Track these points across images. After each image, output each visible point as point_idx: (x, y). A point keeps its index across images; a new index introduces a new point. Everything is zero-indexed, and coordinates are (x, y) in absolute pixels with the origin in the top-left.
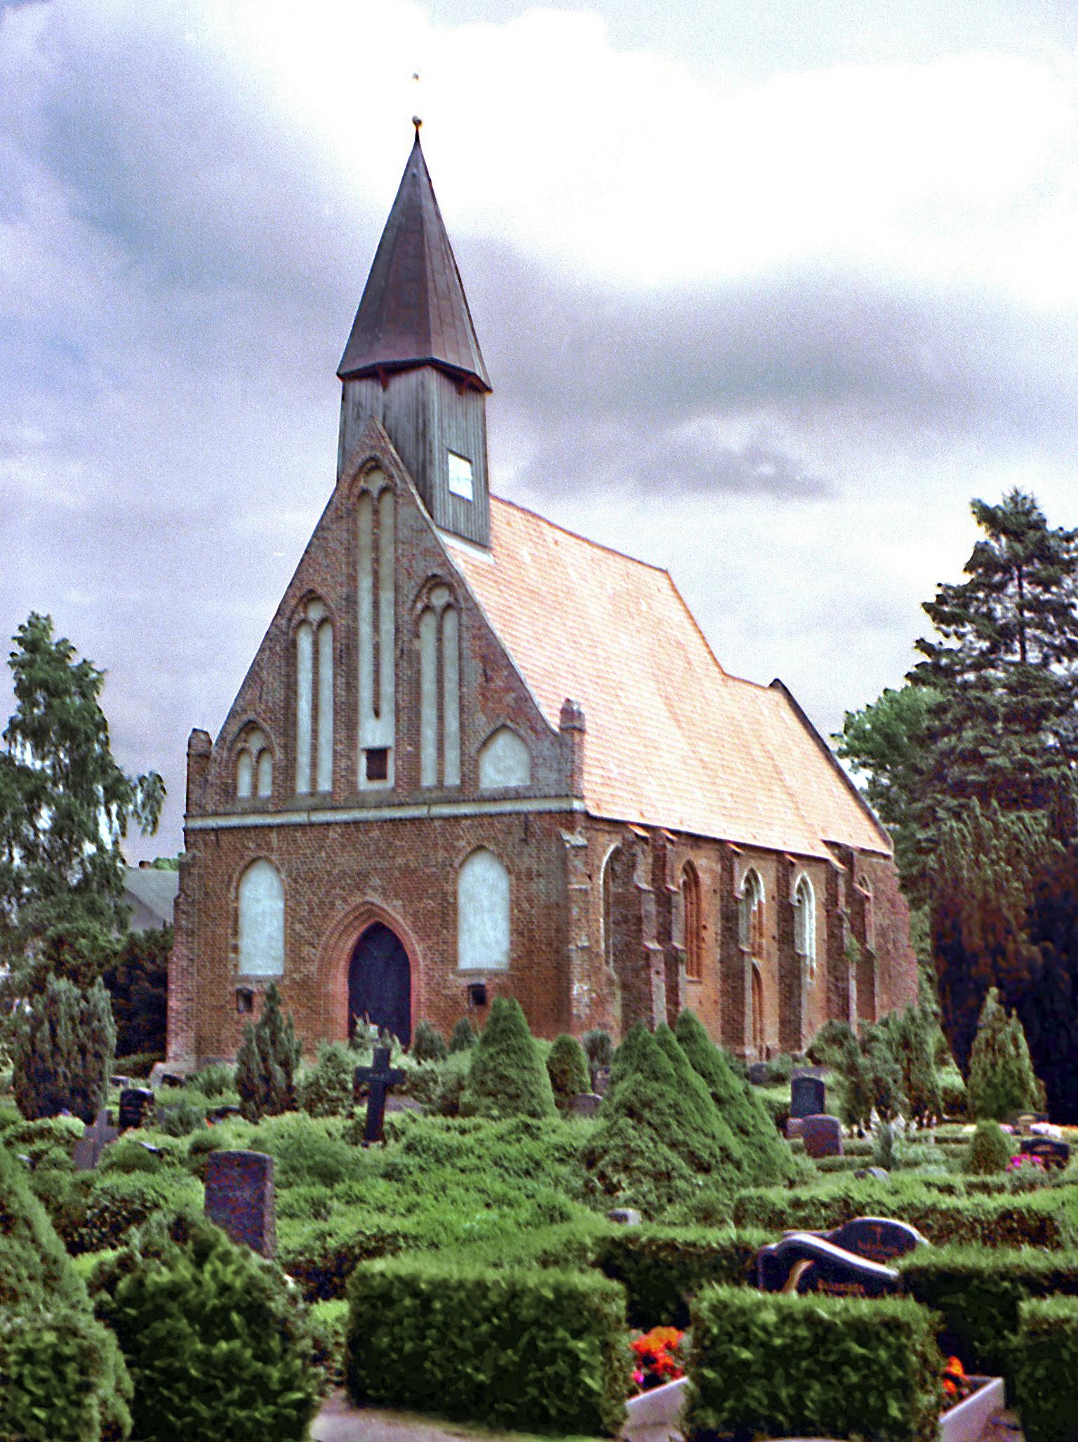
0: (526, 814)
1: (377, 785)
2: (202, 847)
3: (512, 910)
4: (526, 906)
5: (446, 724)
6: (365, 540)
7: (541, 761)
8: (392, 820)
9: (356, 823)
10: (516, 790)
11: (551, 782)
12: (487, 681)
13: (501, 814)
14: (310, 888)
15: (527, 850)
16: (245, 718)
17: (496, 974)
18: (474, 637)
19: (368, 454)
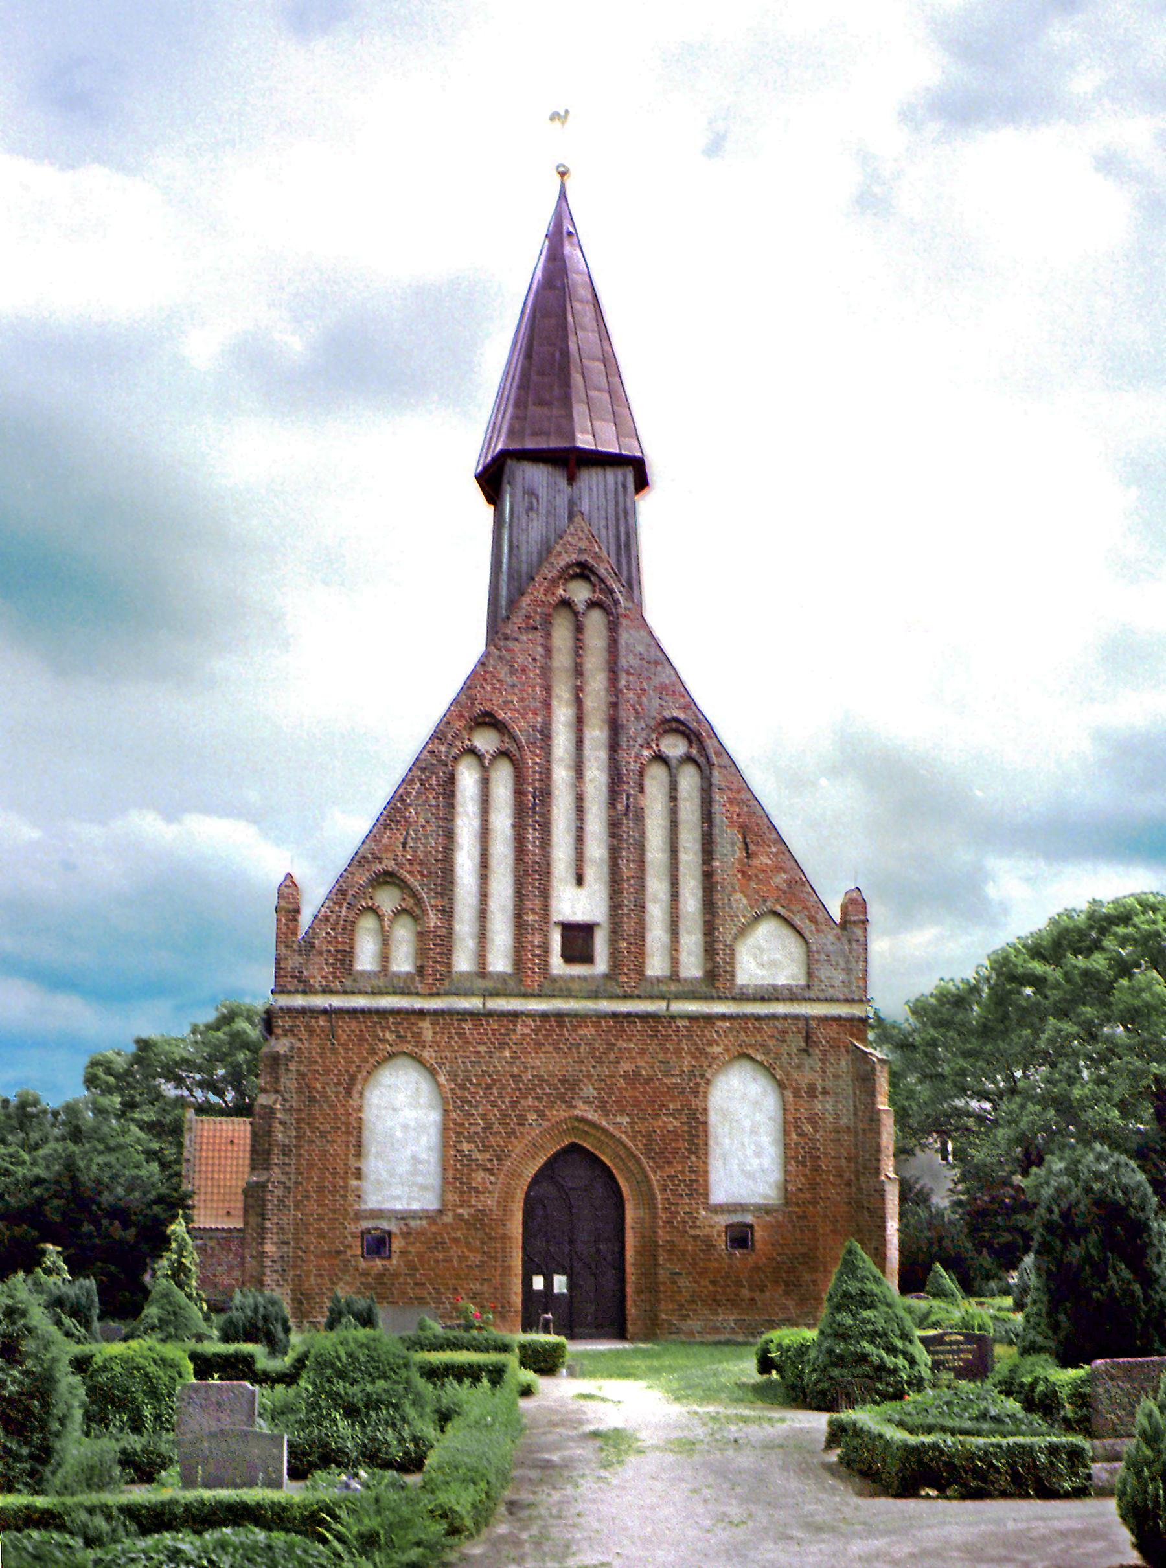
0: (807, 1019)
1: (578, 970)
2: (304, 1034)
3: (786, 1133)
4: (808, 1128)
5: (681, 899)
6: (562, 660)
7: (823, 957)
8: (615, 1015)
9: (559, 1016)
10: (789, 988)
11: (837, 983)
12: (749, 856)
13: (774, 1017)
14: (486, 1096)
15: (808, 1062)
16: (379, 867)
17: (763, 1210)
18: (731, 801)
19: (574, 557)
